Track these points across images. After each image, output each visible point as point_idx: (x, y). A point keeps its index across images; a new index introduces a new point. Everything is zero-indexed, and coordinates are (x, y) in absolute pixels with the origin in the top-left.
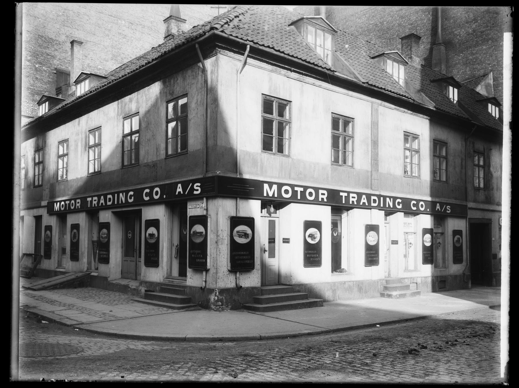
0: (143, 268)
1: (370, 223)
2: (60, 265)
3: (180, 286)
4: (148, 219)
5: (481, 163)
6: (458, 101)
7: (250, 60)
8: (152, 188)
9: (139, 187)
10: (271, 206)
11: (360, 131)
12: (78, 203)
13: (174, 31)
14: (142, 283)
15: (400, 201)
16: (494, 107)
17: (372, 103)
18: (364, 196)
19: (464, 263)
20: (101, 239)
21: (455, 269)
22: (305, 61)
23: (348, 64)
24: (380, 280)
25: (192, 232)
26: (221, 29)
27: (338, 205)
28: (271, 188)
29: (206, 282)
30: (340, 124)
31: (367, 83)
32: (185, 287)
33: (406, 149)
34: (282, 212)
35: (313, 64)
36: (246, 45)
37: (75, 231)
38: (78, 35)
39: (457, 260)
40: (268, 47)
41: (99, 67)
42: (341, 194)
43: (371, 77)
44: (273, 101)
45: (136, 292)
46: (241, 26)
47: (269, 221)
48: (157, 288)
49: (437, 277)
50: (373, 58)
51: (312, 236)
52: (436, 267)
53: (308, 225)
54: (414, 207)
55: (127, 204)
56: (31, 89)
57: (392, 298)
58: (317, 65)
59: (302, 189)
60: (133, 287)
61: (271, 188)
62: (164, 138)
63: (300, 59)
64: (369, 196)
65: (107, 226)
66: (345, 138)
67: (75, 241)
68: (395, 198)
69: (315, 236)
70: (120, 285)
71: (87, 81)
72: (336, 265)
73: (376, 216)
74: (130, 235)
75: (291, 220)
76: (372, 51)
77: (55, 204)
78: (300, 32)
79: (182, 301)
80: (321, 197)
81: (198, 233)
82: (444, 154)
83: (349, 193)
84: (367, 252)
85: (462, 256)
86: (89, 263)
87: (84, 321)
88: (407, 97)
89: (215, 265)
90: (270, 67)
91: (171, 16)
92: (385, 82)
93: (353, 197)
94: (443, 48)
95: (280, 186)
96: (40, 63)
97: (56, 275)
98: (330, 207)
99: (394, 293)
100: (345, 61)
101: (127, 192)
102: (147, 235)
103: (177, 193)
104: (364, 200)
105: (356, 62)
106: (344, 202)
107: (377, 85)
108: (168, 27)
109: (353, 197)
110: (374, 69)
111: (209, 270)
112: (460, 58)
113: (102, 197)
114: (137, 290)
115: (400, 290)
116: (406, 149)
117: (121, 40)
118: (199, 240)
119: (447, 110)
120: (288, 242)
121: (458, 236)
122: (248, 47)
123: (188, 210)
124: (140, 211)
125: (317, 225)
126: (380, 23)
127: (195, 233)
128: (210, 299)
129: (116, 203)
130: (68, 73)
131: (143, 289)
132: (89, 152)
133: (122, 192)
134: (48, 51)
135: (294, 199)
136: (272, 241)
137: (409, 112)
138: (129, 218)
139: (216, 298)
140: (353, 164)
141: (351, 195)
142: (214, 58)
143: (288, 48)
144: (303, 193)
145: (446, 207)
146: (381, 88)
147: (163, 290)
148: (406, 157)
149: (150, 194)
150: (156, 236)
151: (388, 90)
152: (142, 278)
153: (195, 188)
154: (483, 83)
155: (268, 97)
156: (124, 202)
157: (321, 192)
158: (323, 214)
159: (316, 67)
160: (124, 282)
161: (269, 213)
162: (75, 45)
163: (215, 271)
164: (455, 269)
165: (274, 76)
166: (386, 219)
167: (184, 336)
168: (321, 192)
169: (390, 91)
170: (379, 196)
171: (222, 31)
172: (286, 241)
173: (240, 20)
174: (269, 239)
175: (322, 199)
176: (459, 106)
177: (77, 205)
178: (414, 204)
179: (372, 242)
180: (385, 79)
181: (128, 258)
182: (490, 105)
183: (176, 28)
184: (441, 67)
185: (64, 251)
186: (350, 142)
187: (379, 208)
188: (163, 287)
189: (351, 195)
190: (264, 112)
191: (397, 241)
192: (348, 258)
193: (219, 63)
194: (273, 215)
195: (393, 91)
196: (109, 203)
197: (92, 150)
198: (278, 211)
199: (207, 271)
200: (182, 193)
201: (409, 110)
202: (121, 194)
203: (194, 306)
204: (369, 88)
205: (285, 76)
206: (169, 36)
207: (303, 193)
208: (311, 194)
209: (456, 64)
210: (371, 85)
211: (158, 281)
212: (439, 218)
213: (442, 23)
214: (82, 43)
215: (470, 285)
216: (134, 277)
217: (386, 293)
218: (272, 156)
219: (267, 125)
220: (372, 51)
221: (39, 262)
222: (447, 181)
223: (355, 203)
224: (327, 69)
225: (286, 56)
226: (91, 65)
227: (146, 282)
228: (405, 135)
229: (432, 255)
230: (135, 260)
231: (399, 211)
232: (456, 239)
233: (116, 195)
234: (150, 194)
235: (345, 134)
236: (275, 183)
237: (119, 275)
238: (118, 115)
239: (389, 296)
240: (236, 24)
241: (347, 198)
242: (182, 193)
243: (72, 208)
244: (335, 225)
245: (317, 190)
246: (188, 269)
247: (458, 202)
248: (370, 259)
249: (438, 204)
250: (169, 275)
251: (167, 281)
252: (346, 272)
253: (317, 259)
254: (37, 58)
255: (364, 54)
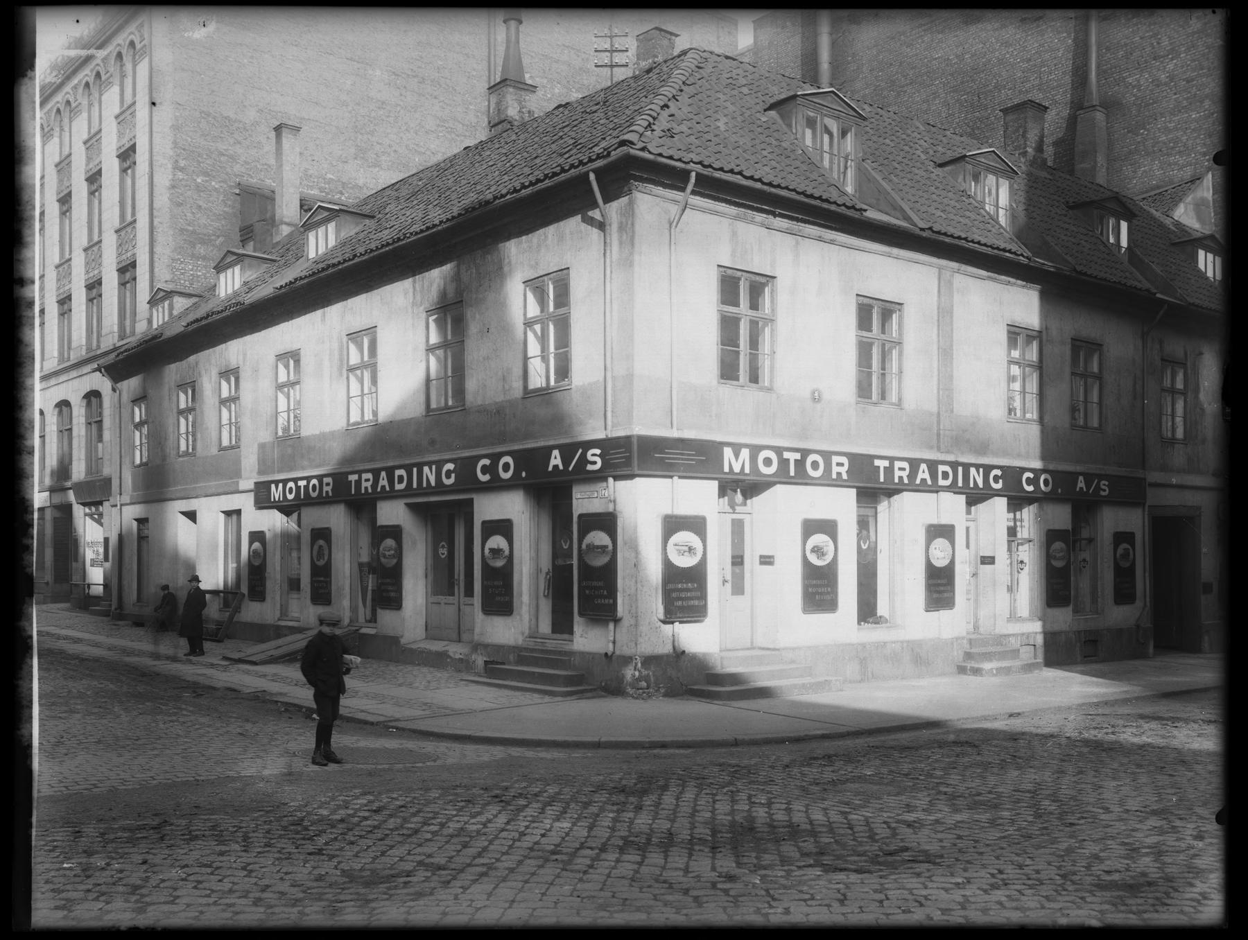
0: (479, 616)
1: (935, 522)
2: (284, 613)
3: (560, 653)
4: (488, 518)
5: (1180, 385)
6: (1129, 248)
7: (697, 200)
8: (495, 458)
9: (466, 453)
10: (735, 491)
11: (915, 330)
12: (328, 484)
13: (512, 112)
14: (476, 647)
15: (998, 472)
16: (1210, 256)
17: (940, 268)
18: (923, 466)
19: (1139, 603)
20: (383, 560)
21: (1119, 616)
22: (803, 193)
23: (888, 188)
24: (957, 639)
25: (584, 546)
26: (640, 145)
27: (872, 488)
28: (737, 456)
29: (614, 642)
30: (874, 314)
31: (930, 228)
32: (571, 653)
33: (1011, 362)
34: (757, 502)
35: (820, 198)
36: (688, 172)
37: (321, 542)
38: (290, 110)
39: (1124, 595)
40: (731, 171)
41: (329, 176)
42: (877, 462)
43: (939, 213)
44: (739, 279)
45: (463, 666)
46: (677, 129)
47: (733, 520)
48: (511, 657)
49: (1079, 632)
50: (941, 165)
51: (818, 550)
52: (1075, 611)
53: (811, 527)
54: (1028, 484)
55: (440, 488)
56: (187, 230)
57: (981, 675)
58: (827, 201)
59: (798, 456)
60: (457, 656)
61: (737, 456)
62: (520, 356)
63: (794, 190)
64: (933, 466)
65: (395, 532)
66: (883, 345)
67: (321, 563)
68: (988, 469)
69: (825, 549)
70: (430, 652)
71: (331, 227)
72: (867, 611)
73: (951, 507)
74: (443, 552)
75: (779, 516)
76: (940, 148)
77: (273, 486)
78: (790, 126)
79: (569, 681)
80: (835, 469)
81: (598, 547)
82: (1096, 370)
83: (892, 460)
84: (932, 582)
85: (1134, 587)
86: (354, 609)
87: (398, 716)
88: (1015, 253)
89: (633, 611)
90: (733, 210)
91: (504, 81)
92: (967, 221)
93: (900, 469)
94: (1099, 116)
95: (755, 450)
96: (206, 174)
97: (278, 636)
98: (854, 490)
99: (987, 666)
100: (884, 183)
101: (440, 464)
102: (487, 551)
103: (550, 469)
104: (923, 473)
105: (906, 181)
106: (882, 480)
107: (951, 230)
108: (498, 103)
109: (900, 469)
110: (944, 193)
111: (620, 620)
112: (1139, 139)
113: (383, 474)
114: (467, 661)
115: (999, 660)
116: (1011, 362)
117: (373, 114)
118: (600, 561)
119: (1102, 275)
120: (771, 563)
121: (1125, 546)
122: (693, 174)
123: (574, 501)
124: (470, 502)
125: (829, 528)
126: (957, 56)
127: (592, 548)
128: (623, 676)
129: (415, 485)
130: (267, 193)
131: (480, 660)
132: (348, 378)
133: (429, 464)
134: (222, 147)
135: (783, 477)
136: (738, 561)
137: (1019, 282)
138: (445, 515)
139: (637, 673)
140: (900, 400)
141: (898, 464)
142: (624, 200)
143: (767, 169)
144: (800, 464)
145: (1098, 483)
146: (959, 238)
147: (522, 660)
148: (1012, 379)
149: (491, 470)
150: (507, 553)
151: (972, 241)
152: (476, 638)
153: (590, 458)
154: (1189, 199)
155: (729, 272)
156: (433, 483)
157: (835, 459)
158: (841, 505)
159: (825, 205)
160: (437, 646)
161: (732, 505)
162: (285, 133)
163: (633, 622)
164: (1119, 616)
165: (741, 226)
166: (968, 512)
167: (596, 739)
168: (835, 459)
169: (979, 243)
170: (954, 465)
171: (643, 149)
172: (767, 560)
173: (672, 115)
174: (733, 557)
175: (839, 474)
176: (1131, 261)
177: (326, 489)
178: (1028, 479)
179: (940, 561)
180: (968, 213)
181: (441, 599)
182: (1201, 253)
183: (516, 105)
184: (1095, 162)
185: (294, 585)
186: (895, 353)
187: (953, 488)
188: (522, 655)
189: (898, 464)
190: (723, 302)
191: (993, 558)
192: (892, 594)
193: (637, 211)
194: (738, 509)
195: (983, 241)
196: (398, 487)
197: (356, 376)
198: (749, 501)
199: (617, 621)
200: (561, 467)
201: (1017, 278)
202: (426, 469)
203: (591, 690)
204: (935, 240)
205: (762, 225)
206: (499, 123)
207: (800, 464)
208: (815, 465)
209: (1130, 152)
210: (939, 233)
211: (512, 642)
212: (1084, 508)
213: (1098, 57)
214: (298, 129)
215: (1151, 650)
216: (455, 636)
217: (969, 666)
218: (739, 391)
219: (729, 326)
220: (940, 148)
221: (237, 610)
222: (1100, 428)
223: (906, 481)
224: (848, 208)
225: (765, 188)
226: (310, 172)
227: (486, 646)
228: (1009, 332)
229: (1067, 585)
230: (456, 602)
231: (998, 494)
232: (1120, 551)
233: (415, 470)
234: (491, 470)
235: (883, 337)
236: (746, 446)
237: (420, 633)
238: (414, 304)
239: (977, 672)
240: (666, 126)
241: (889, 471)
242: (561, 467)
243: (314, 495)
244: (863, 524)
245: (827, 455)
246: (577, 618)
247: (1122, 472)
248: (935, 596)
249: (1081, 478)
250: (533, 635)
251: (531, 644)
252: (886, 621)
253: (828, 597)
254: (199, 162)
255: (923, 157)
